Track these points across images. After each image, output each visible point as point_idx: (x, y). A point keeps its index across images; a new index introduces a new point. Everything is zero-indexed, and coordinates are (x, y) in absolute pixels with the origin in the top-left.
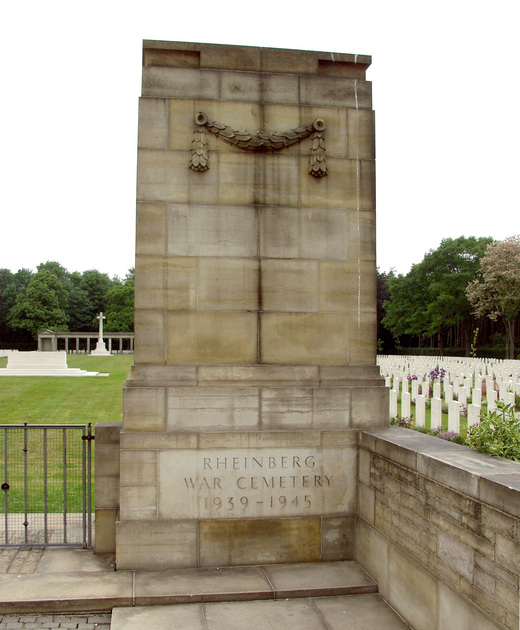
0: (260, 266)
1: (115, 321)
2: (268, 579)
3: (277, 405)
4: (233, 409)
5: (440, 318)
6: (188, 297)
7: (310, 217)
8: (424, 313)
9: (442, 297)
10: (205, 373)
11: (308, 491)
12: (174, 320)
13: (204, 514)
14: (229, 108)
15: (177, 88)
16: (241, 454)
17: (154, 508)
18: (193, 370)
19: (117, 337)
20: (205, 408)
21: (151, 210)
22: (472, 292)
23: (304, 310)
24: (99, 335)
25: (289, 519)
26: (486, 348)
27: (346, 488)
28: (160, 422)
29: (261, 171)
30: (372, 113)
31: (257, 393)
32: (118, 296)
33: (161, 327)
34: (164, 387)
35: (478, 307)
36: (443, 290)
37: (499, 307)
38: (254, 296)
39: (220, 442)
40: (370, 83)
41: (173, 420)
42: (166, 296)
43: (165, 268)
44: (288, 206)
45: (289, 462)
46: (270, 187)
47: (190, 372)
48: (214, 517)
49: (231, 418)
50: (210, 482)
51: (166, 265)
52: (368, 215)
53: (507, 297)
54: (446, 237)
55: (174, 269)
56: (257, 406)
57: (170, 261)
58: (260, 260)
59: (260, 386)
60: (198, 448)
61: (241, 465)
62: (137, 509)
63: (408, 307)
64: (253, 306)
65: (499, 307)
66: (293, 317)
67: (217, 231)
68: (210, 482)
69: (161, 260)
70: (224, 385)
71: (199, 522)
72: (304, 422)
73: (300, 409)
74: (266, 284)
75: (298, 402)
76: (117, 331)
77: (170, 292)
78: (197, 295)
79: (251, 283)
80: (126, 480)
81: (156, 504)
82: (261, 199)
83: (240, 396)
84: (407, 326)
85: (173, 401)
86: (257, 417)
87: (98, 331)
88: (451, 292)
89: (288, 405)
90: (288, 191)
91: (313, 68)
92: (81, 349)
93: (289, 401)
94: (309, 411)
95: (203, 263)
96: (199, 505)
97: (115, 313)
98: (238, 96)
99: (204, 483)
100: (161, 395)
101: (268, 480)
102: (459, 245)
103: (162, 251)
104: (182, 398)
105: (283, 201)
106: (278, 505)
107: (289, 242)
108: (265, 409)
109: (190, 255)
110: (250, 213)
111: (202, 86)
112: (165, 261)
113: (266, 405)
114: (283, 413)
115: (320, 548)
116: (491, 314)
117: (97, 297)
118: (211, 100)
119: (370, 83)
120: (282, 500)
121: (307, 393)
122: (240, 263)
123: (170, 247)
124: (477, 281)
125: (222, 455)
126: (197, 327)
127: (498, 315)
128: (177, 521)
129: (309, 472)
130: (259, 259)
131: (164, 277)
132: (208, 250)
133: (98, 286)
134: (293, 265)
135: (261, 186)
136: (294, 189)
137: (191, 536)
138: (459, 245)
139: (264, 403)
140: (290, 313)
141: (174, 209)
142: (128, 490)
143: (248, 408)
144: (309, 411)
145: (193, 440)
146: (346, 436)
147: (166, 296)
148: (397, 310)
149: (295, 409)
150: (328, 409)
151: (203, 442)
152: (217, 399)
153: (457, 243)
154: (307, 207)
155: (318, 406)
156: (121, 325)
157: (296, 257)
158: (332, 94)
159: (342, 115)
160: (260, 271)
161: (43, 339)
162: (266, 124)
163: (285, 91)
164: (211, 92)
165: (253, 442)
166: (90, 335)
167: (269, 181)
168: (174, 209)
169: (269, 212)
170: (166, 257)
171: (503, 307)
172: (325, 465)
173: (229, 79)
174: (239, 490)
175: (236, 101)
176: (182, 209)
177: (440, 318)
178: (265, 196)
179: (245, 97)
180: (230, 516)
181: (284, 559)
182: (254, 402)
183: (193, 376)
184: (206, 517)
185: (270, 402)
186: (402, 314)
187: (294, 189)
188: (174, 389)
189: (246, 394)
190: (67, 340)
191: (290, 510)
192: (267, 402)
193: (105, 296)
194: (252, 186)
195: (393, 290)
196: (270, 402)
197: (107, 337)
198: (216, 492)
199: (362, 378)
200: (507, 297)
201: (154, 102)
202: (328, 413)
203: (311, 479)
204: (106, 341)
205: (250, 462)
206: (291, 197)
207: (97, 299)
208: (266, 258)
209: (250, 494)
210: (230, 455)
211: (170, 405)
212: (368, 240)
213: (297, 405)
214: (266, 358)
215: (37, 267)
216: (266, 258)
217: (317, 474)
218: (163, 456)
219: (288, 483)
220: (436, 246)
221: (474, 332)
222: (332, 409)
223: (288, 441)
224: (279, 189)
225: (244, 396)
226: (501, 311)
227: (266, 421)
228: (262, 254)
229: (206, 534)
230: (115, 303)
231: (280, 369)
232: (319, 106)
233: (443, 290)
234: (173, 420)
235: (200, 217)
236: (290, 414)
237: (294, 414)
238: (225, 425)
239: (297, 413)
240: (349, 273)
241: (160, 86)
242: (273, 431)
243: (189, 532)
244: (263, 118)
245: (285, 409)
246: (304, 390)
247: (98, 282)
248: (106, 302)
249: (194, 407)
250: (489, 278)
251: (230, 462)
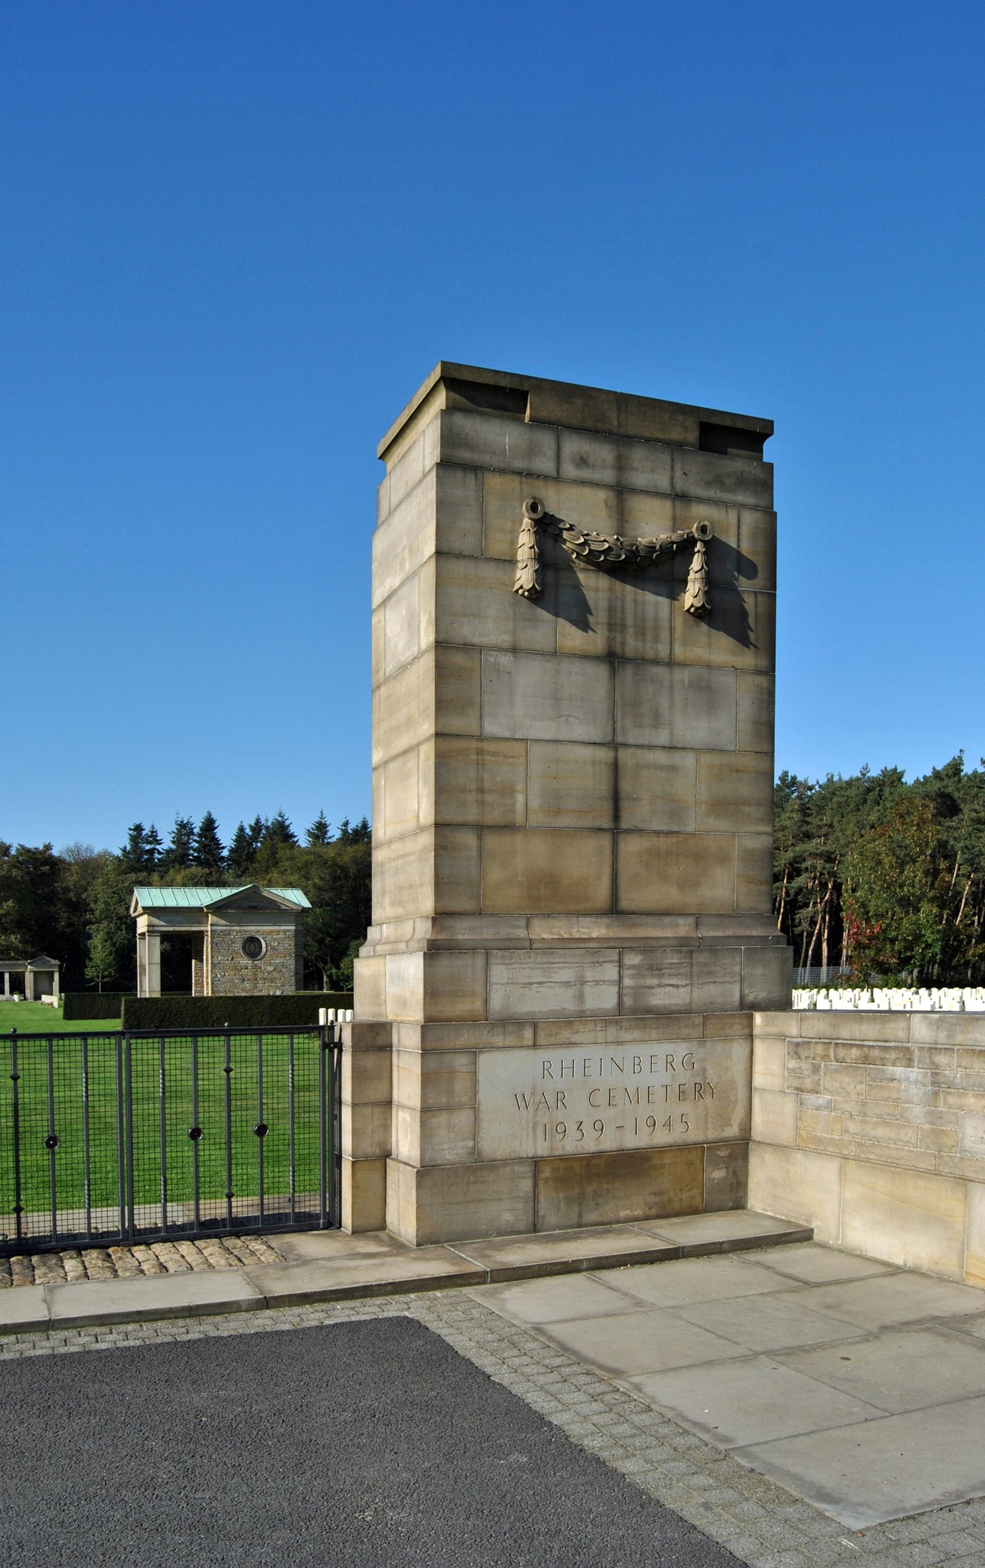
0: (616, 758)
2: (455, 1260)
3: (644, 976)
4: (583, 983)
6: (514, 804)
7: (686, 680)
10: (542, 930)
11: (686, 1107)
12: (493, 842)
13: (542, 1149)
14: (572, 493)
15: (494, 453)
16: (595, 1053)
17: (470, 1144)
18: (523, 922)
20: (544, 983)
21: (459, 659)
23: (675, 828)
25: (662, 1150)
27: (736, 1100)
28: (478, 1005)
29: (619, 604)
30: (774, 515)
31: (616, 958)
33: (474, 853)
34: (486, 950)
38: (607, 806)
39: (565, 1035)
40: (771, 466)
41: (497, 1002)
42: (482, 803)
43: (480, 757)
44: (656, 662)
45: (661, 1063)
46: (631, 631)
47: (518, 927)
48: (557, 1153)
49: (581, 997)
50: (551, 1100)
51: (481, 752)
52: (763, 681)
55: (493, 759)
56: (616, 978)
57: (487, 746)
58: (616, 749)
59: (622, 947)
60: (535, 1046)
61: (594, 1069)
62: (446, 1146)
64: (606, 823)
66: (662, 839)
67: (557, 699)
68: (551, 1100)
69: (474, 744)
70: (570, 946)
71: (536, 1163)
72: (680, 1001)
73: (674, 981)
74: (626, 786)
75: (672, 971)
77: (489, 798)
78: (527, 801)
79: (604, 787)
80: (430, 1101)
81: (474, 1136)
82: (618, 650)
83: (593, 963)
85: (499, 973)
86: (616, 996)
89: (659, 975)
90: (656, 639)
91: (692, 436)
93: (660, 969)
94: (687, 985)
95: (536, 750)
96: (535, 1136)
98: (585, 474)
99: (543, 1099)
100: (480, 961)
101: (632, 1093)
103: (474, 729)
104: (511, 967)
105: (650, 654)
106: (644, 1131)
107: (657, 722)
108: (627, 982)
109: (517, 737)
110: (601, 672)
111: (532, 451)
112: (480, 745)
113: (629, 975)
114: (652, 987)
115: (702, 1193)
118: (546, 478)
119: (771, 466)
120: (650, 1122)
121: (685, 958)
122: (587, 753)
123: (486, 724)
125: (566, 1055)
126: (528, 854)
128: (506, 1162)
129: (684, 1077)
130: (614, 745)
131: (478, 771)
132: (543, 730)
134: (661, 758)
135: (618, 628)
136: (665, 635)
137: (526, 1185)
139: (626, 973)
140: (658, 833)
141: (492, 659)
142: (432, 1117)
143: (604, 981)
144: (687, 985)
145: (528, 1033)
146: (737, 1021)
147: (482, 803)
149: (669, 982)
150: (712, 980)
151: (542, 1036)
152: (560, 968)
154: (684, 665)
155: (699, 976)
157: (666, 744)
158: (718, 481)
159: (732, 515)
160: (615, 767)
162: (626, 525)
163: (653, 471)
164: (545, 464)
165: (612, 1033)
167: (630, 620)
168: (492, 659)
169: (629, 671)
170: (481, 738)
172: (708, 1067)
173: (573, 445)
174: (591, 1109)
175: (582, 483)
176: (505, 660)
178: (623, 644)
179: (597, 476)
180: (579, 1150)
181: (654, 1212)
182: (611, 972)
183: (522, 933)
184: (546, 1154)
185: (634, 972)
187: (665, 635)
188: (499, 953)
189: (601, 960)
191: (661, 1138)
192: (631, 972)
194: (606, 627)
196: (634, 972)
198: (560, 1115)
199: (754, 933)
201: (459, 474)
202: (712, 987)
203: (689, 1087)
205: (607, 1064)
206: (660, 647)
208: (625, 745)
209: (606, 1114)
210: (577, 1054)
211: (494, 979)
212: (764, 720)
213: (670, 975)
214: (624, 904)
216: (625, 745)
217: (698, 1080)
218: (484, 1060)
219: (659, 1095)
222: (718, 980)
223: (660, 1031)
224: (643, 635)
225: (598, 963)
227: (628, 1001)
228: (619, 739)
229: (546, 1180)
231: (644, 919)
232: (700, 500)
234: (497, 1002)
235: (531, 675)
236: (662, 989)
237: (667, 989)
238: (571, 1008)
239: (671, 989)
240: (738, 771)
241: (470, 447)
242: (637, 1016)
243: (523, 1178)
244: (621, 517)
245: (655, 982)
246: (682, 952)
249: (527, 981)
251: (578, 1068)
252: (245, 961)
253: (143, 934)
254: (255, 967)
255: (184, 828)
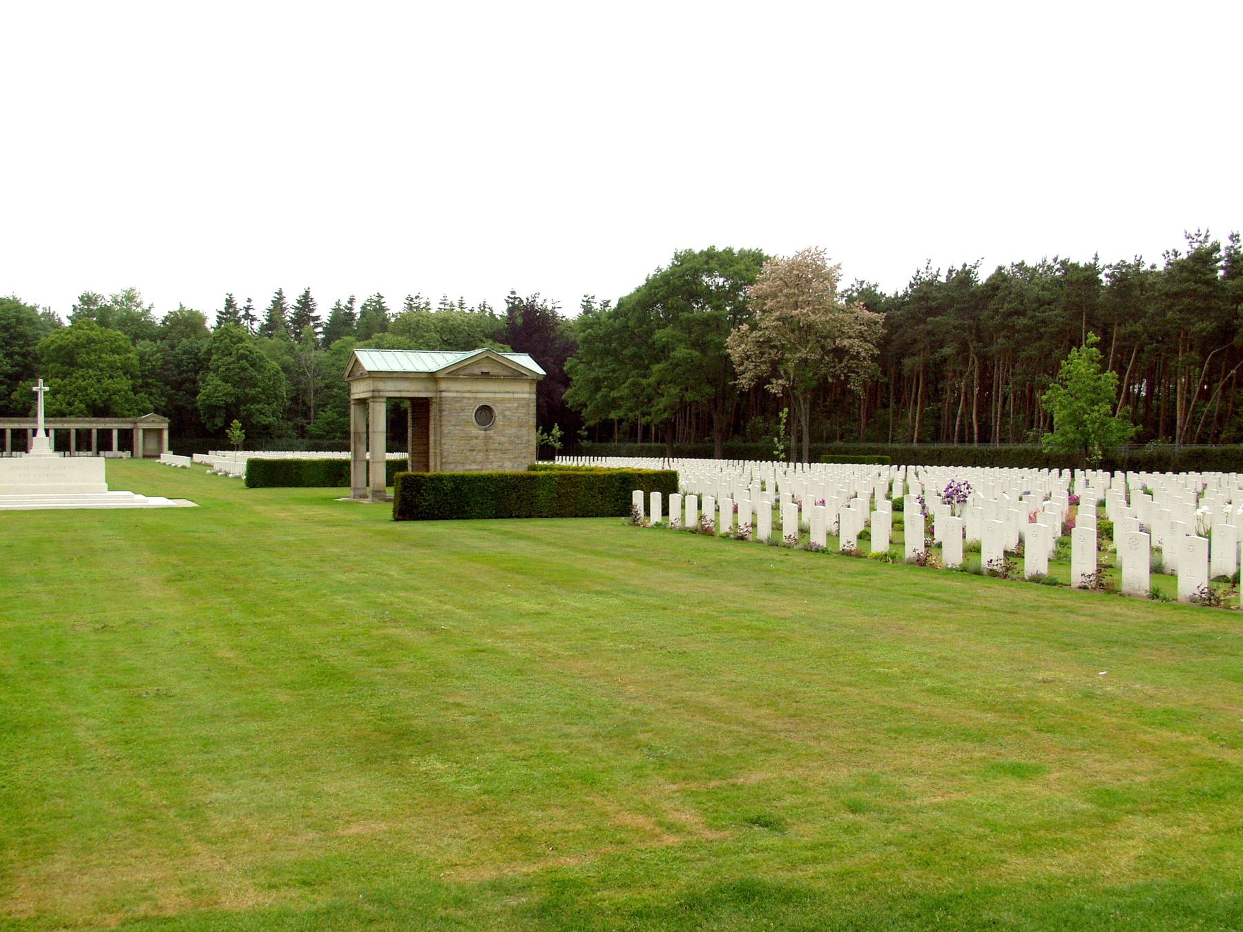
1: (59, 396)
5: (675, 390)
8: (644, 382)
9: (681, 352)
19: (66, 426)
22: (737, 345)
24: (36, 422)
26: (736, 442)
32: (61, 348)
35: (744, 373)
36: (680, 341)
37: (786, 373)
53: (798, 355)
54: (682, 248)
63: (614, 371)
65: (786, 373)
76: (64, 415)
84: (613, 404)
87: (36, 415)
88: (694, 345)
92: (121, 448)
97: (59, 380)
102: (707, 263)
116: (770, 383)
117: (17, 349)
124: (745, 327)
127: (784, 386)
133: (20, 329)
138: (707, 263)
148: (593, 375)
153: (705, 258)
156: (70, 404)
161: (145, 430)
166: (12, 422)
171: (791, 371)
177: (675, 390)
186: (597, 384)
190: (94, 433)
193: (37, 348)
195: (585, 341)
197: (48, 426)
200: (798, 355)
204: (47, 432)
207: (18, 353)
215: (130, 297)
220: (666, 263)
221: (781, 414)
226: (788, 379)
230: (55, 361)
233: (680, 341)
247: (19, 321)
248: (36, 359)
250: (769, 321)
252: (475, 431)
253: (363, 402)
254: (487, 438)
255: (278, 303)
